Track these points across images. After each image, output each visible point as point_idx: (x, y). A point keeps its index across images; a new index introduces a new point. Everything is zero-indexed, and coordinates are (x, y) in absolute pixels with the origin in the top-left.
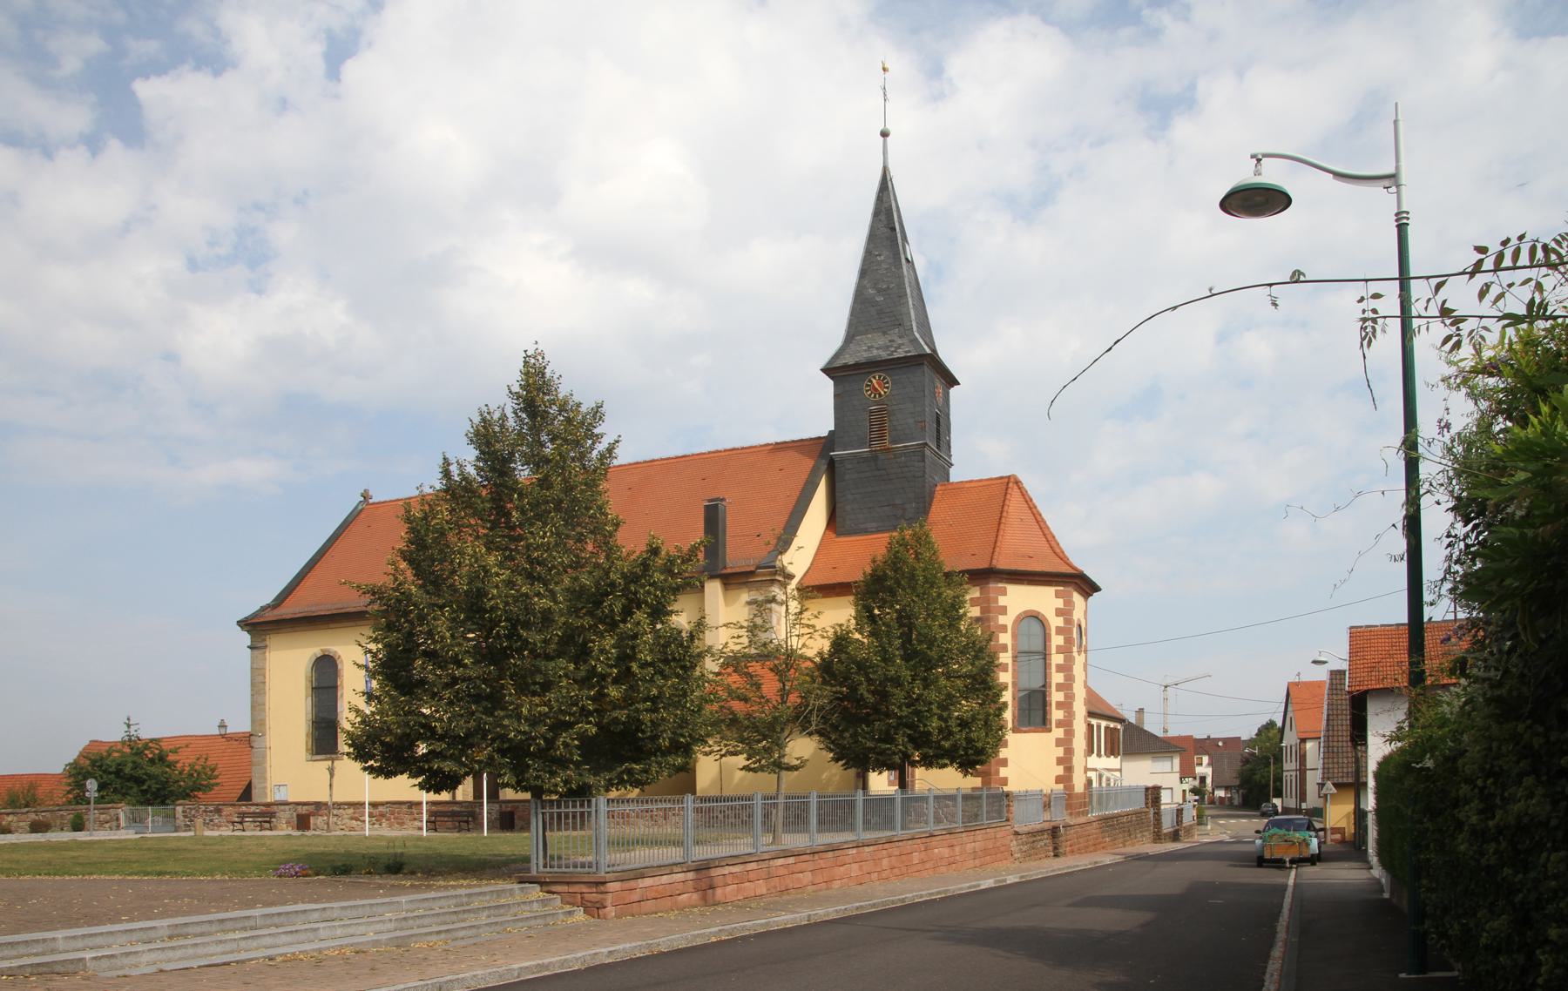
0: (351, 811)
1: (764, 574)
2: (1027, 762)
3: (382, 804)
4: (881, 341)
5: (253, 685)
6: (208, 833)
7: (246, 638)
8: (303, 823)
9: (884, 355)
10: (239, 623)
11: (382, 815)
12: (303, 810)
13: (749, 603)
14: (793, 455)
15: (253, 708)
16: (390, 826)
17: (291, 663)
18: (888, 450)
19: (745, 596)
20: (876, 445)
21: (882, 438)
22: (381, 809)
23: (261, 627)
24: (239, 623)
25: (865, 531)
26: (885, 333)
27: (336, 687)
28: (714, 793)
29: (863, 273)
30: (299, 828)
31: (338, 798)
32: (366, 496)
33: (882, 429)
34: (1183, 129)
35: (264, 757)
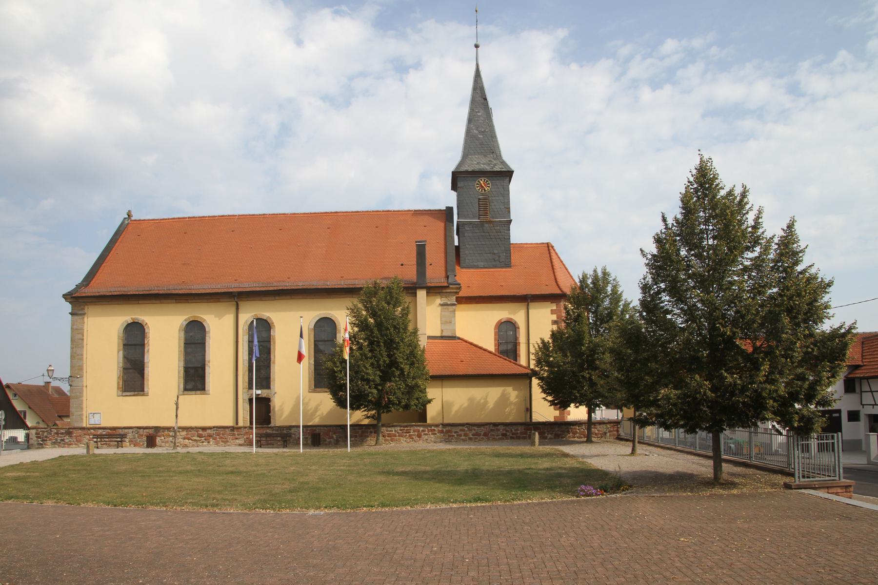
0: (184, 433)
1: (452, 288)
2: (445, 401)
3: (210, 428)
4: (484, 160)
5: (72, 341)
6: (97, 451)
7: (68, 307)
8: (151, 442)
9: (488, 168)
10: (65, 296)
11: (210, 436)
12: (151, 431)
13: (441, 305)
14: (427, 219)
15: (72, 357)
16: (217, 444)
17: (105, 329)
18: (490, 222)
19: (438, 301)
20: (483, 218)
21: (486, 214)
22: (209, 431)
23: (81, 300)
24: (65, 296)
25: (477, 267)
26: (485, 156)
27: (143, 345)
28: (439, 421)
29: (470, 121)
30: (148, 446)
31: (184, 422)
32: (129, 215)
33: (485, 209)
34: (413, 77)
35: (81, 392)
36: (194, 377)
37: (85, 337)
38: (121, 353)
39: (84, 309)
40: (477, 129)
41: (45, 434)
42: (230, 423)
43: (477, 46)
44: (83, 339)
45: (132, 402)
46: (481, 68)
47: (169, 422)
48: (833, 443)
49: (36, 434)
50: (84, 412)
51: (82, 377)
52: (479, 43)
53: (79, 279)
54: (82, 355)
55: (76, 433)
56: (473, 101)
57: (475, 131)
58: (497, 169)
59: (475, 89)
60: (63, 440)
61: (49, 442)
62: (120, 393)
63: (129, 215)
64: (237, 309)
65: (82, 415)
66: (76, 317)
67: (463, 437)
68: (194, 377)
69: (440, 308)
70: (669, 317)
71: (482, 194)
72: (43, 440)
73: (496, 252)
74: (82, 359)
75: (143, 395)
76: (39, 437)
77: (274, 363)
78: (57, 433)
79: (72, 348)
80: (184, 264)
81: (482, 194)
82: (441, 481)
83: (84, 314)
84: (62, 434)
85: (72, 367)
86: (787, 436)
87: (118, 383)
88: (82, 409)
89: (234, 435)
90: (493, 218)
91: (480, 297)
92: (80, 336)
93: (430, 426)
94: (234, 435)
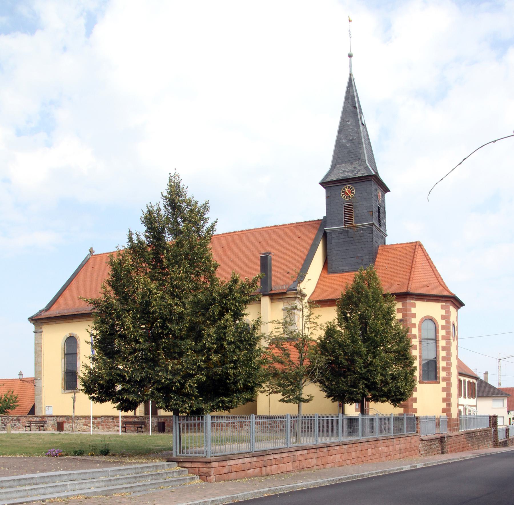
1: (291, 294)
2: (427, 400)
3: (99, 417)
4: (350, 167)
5: (36, 352)
8: (60, 427)
9: (351, 175)
11: (99, 423)
12: (60, 420)
15: (36, 365)
21: (350, 220)
22: (98, 419)
23: (40, 321)
25: (343, 271)
26: (351, 163)
29: (340, 131)
32: (91, 251)
33: (350, 215)
35: (41, 391)
37: (43, 350)
39: (41, 328)
40: (346, 139)
43: (350, 56)
44: (41, 351)
46: (355, 77)
47: (70, 413)
48: (203, 423)
50: (43, 406)
51: (41, 379)
52: (353, 52)
53: (43, 306)
54: (41, 363)
56: (345, 112)
57: (344, 141)
58: (360, 175)
59: (346, 99)
60: (15, 425)
63: (91, 251)
65: (42, 407)
66: (37, 334)
67: (275, 429)
69: (283, 312)
70: (118, 298)
71: (347, 201)
72: (5, 425)
73: (359, 255)
78: (12, 420)
79: (35, 358)
81: (347, 201)
83: (42, 332)
84: (15, 420)
85: (36, 372)
88: (42, 403)
89: (114, 422)
90: (357, 223)
91: (329, 300)
93: (261, 417)
94: (114, 422)
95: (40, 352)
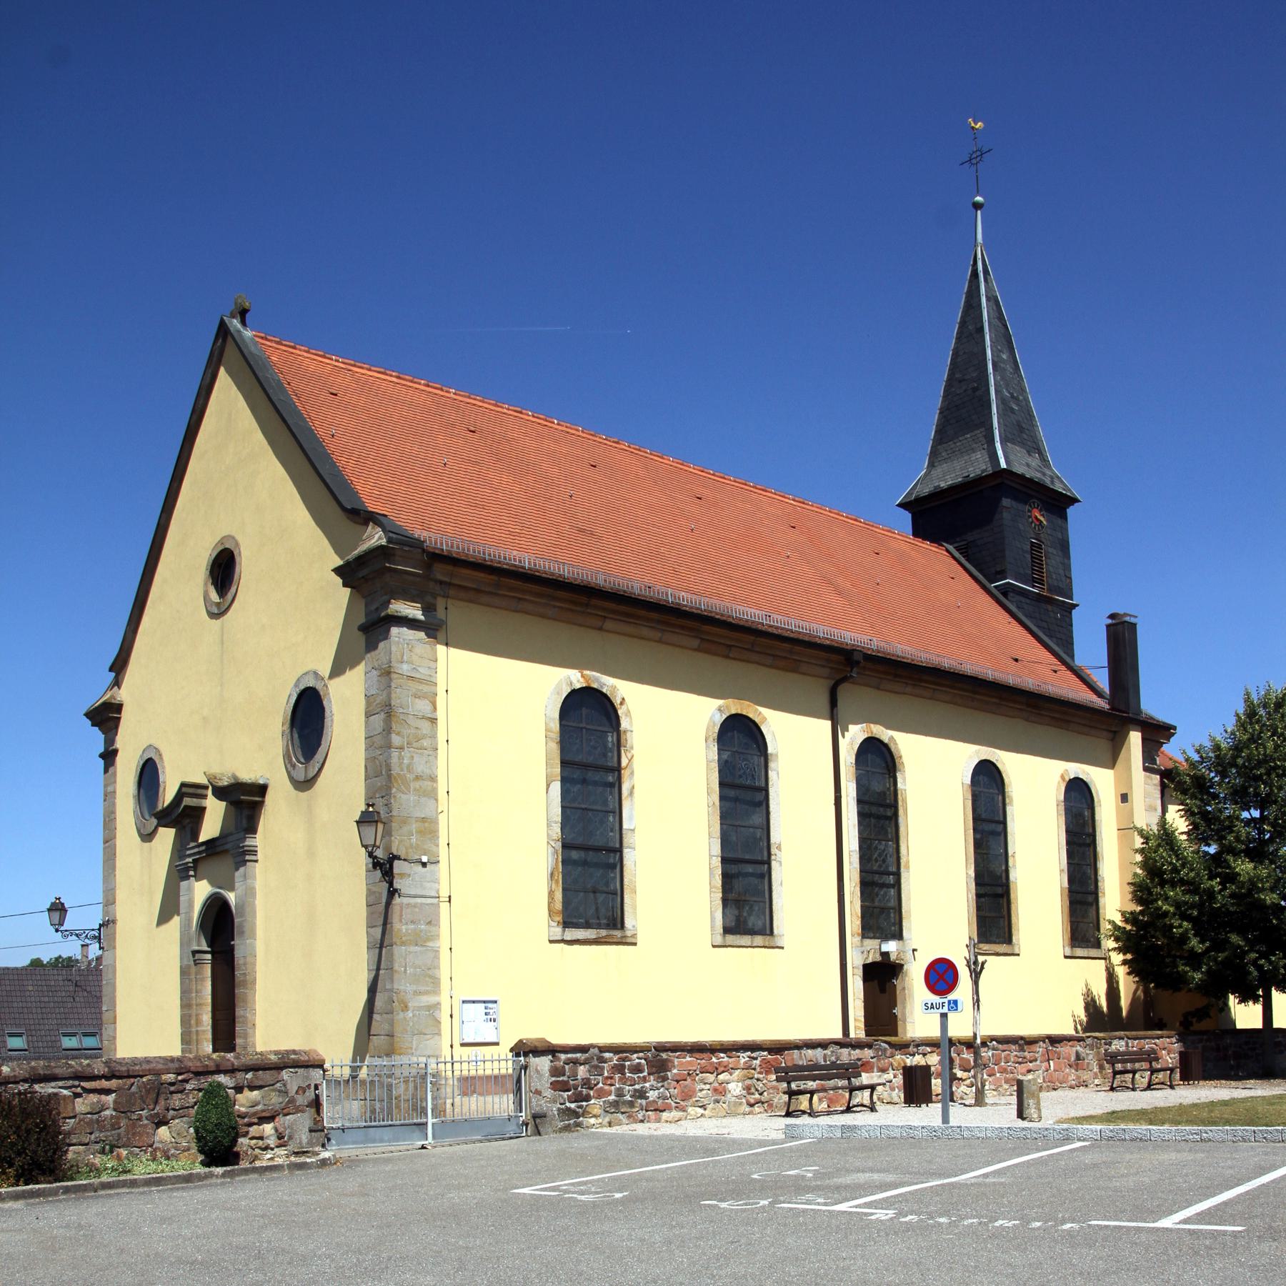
35: (433, 922)
36: (746, 900)
37: (441, 714)
38: (556, 787)
41: (582, 1071)
42: (837, 1034)
44: (433, 721)
45: (746, 958)
49: (555, 1072)
54: (433, 779)
55: (681, 1064)
60: (641, 1094)
61: (595, 1105)
62: (557, 932)
64: (833, 703)
68: (746, 900)
74: (433, 795)
75: (622, 942)
76: (564, 1087)
77: (907, 867)
78: (620, 1069)
80: (581, 530)
82: (734, 1141)
84: (637, 1069)
86: (209, 1058)
87: (551, 893)
88: (436, 982)
92: (422, 706)
95: (425, 726)
